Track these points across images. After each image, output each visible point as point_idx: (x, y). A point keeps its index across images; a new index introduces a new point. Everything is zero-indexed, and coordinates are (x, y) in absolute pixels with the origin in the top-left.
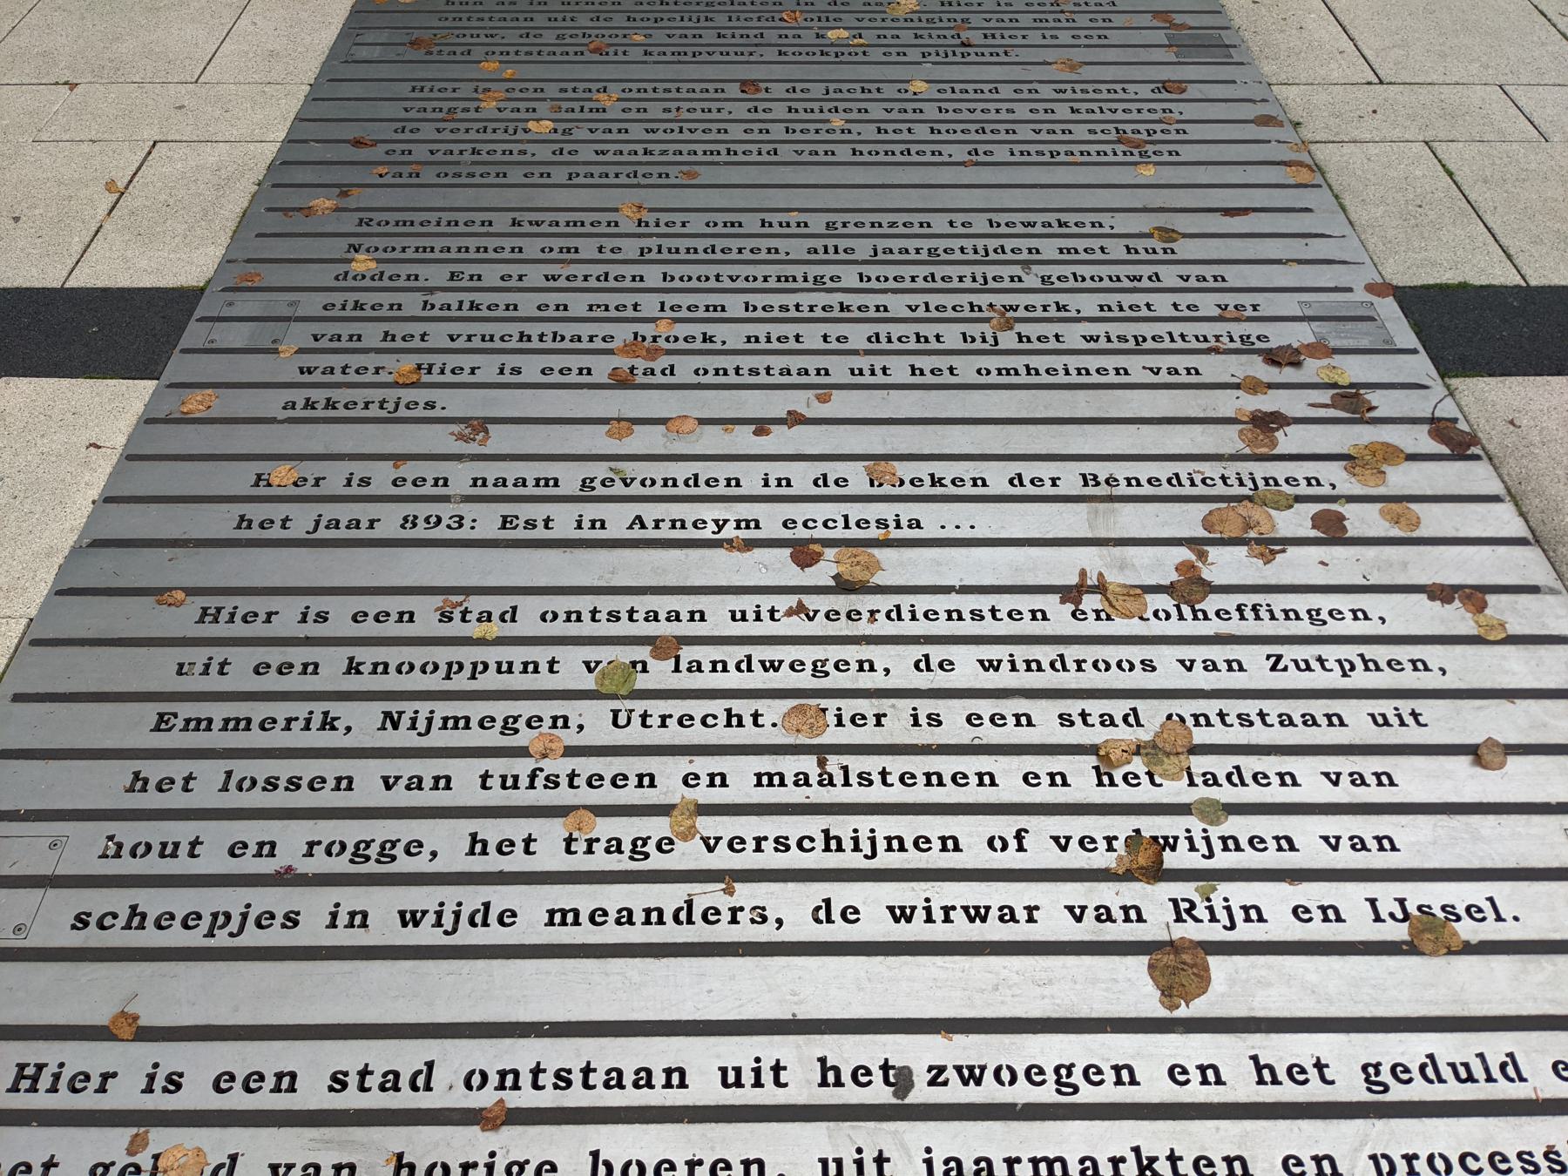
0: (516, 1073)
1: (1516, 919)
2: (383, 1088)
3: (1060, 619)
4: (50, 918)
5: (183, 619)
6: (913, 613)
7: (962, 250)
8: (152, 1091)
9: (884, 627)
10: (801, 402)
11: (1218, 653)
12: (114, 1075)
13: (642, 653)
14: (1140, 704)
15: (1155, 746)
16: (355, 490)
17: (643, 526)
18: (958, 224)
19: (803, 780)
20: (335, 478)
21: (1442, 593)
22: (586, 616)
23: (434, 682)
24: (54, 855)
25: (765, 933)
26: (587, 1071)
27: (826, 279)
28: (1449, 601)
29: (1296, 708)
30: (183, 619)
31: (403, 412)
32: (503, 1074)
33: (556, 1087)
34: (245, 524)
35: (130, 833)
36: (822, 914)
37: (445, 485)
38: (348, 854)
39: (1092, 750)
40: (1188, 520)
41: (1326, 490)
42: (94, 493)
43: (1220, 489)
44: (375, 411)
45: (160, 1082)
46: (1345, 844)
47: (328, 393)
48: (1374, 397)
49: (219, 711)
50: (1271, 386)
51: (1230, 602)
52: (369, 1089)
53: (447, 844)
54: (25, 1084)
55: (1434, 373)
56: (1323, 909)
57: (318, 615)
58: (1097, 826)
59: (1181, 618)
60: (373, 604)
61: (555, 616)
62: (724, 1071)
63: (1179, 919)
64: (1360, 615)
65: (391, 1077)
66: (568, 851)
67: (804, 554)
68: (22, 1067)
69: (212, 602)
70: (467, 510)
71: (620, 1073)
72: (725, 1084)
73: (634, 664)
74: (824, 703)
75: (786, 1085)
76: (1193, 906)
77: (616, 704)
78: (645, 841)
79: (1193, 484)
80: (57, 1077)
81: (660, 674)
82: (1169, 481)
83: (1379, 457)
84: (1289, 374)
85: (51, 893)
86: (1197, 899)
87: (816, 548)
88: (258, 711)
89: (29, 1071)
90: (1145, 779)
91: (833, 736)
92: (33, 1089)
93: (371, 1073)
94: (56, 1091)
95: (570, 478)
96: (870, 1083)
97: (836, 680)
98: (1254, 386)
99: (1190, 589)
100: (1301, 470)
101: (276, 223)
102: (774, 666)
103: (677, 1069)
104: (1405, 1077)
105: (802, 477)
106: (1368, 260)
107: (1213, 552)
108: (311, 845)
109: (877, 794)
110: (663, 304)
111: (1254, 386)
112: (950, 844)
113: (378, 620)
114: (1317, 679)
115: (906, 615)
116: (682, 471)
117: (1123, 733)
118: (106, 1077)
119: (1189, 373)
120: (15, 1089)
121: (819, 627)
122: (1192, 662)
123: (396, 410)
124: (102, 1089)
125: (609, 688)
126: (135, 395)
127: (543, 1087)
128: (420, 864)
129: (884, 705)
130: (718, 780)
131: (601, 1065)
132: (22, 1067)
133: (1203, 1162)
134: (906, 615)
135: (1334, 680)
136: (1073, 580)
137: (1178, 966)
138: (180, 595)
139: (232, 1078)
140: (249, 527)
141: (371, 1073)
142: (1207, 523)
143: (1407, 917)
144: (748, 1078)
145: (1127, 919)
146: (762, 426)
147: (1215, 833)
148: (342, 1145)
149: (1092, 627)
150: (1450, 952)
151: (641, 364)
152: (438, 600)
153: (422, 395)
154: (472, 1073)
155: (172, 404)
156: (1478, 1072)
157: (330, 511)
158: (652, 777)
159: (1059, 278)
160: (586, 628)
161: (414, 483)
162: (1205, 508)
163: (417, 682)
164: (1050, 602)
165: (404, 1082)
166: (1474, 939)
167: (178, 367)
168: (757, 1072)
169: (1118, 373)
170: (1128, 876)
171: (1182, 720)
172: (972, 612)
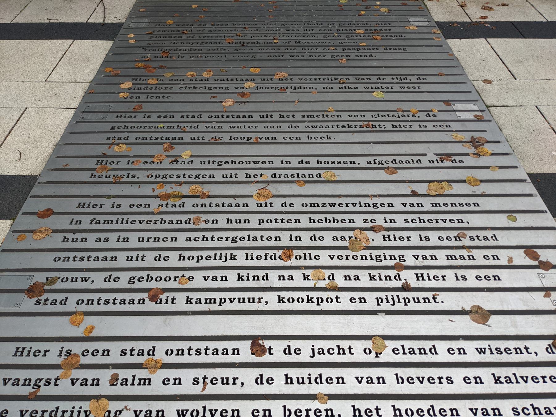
0: (183, 350)
2: (138, 355)
12: (49, 351)
18: (340, 127)
22: (208, 205)
30: (111, 117)
33: (196, 354)
34: (66, 240)
36: (287, 351)
54: (19, 354)
57: (118, 205)
61: (197, 206)
68: (18, 348)
69: (21, 344)
71: (217, 350)
75: (353, 354)
80: (29, 351)
89: (20, 350)
92: (22, 355)
101: (61, 163)
110: (231, 137)
118: (46, 351)
122: (418, 256)
132: (18, 348)
140: (95, 177)
144: (306, 381)
154: (168, 350)
156: (513, 380)
158: (226, 277)
159: (385, 162)
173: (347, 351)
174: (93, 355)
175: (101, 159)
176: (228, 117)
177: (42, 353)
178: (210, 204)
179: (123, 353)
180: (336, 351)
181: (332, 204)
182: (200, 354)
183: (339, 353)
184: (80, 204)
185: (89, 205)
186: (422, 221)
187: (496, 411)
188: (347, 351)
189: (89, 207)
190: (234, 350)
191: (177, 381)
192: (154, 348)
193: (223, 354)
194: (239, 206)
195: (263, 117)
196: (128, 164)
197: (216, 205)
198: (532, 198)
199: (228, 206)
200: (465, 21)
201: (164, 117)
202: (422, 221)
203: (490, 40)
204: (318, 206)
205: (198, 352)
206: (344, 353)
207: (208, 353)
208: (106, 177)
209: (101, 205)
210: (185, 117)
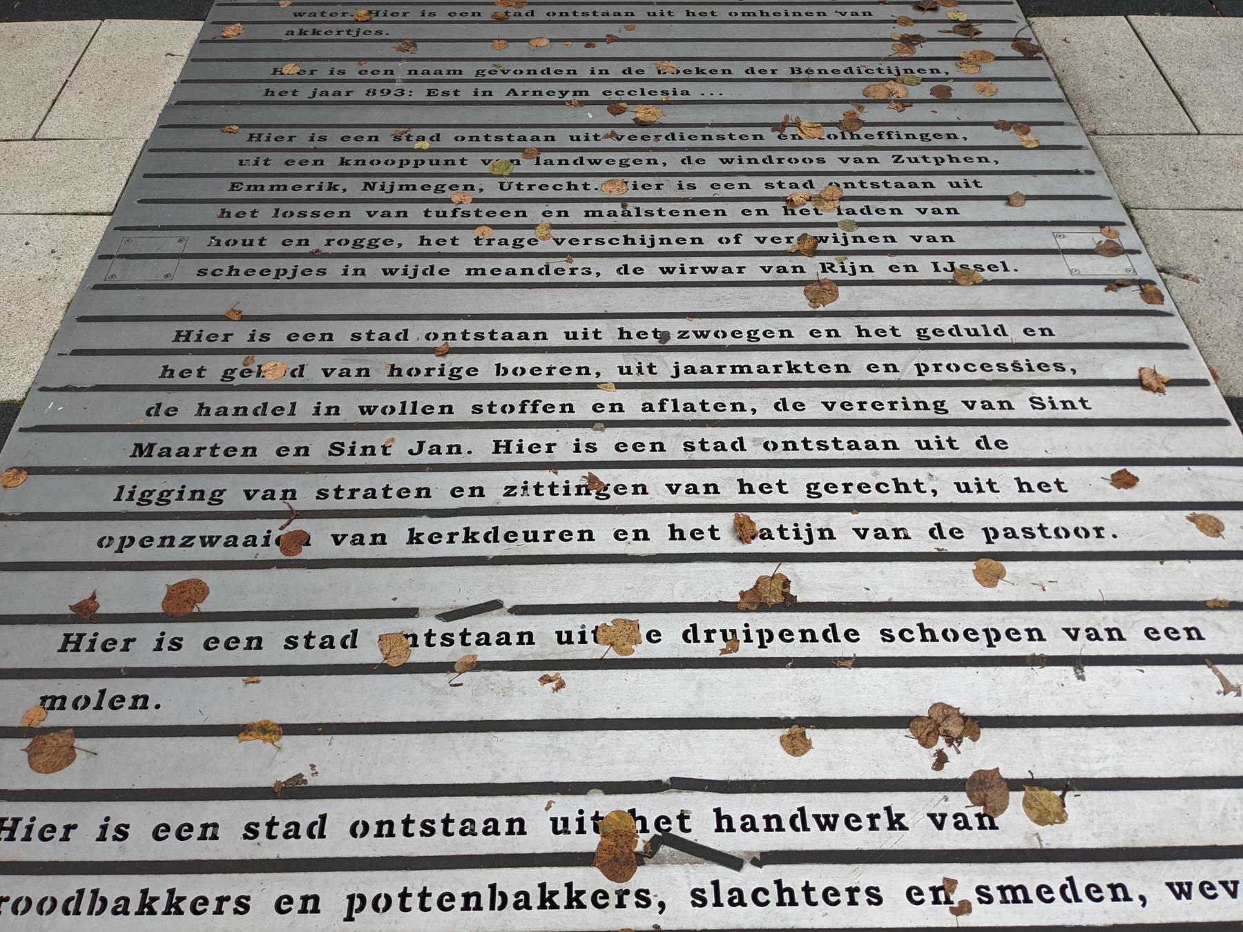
0: (391, 824)
2: (286, 836)
3: (771, 138)
5: (241, 139)
8: (104, 839)
9: (663, 143)
10: (614, 30)
11: (863, 155)
13: (518, 156)
14: (814, 179)
15: (820, 197)
16: (335, 76)
17: (515, 94)
19: (613, 214)
20: (323, 70)
21: (1003, 126)
23: (395, 169)
24: (182, 244)
25: (591, 278)
26: (447, 821)
28: (1008, 129)
29: (906, 180)
31: (361, 36)
32: (380, 824)
33: (422, 834)
35: (224, 236)
37: (331, 339)
38: (351, 244)
39: (784, 199)
40: (855, 91)
41: (943, 75)
42: (175, 79)
43: (877, 75)
44: (344, 36)
45: (110, 833)
47: (314, 26)
48: (980, 27)
49: (267, 182)
50: (915, 21)
51: (874, 131)
52: (275, 837)
53: (409, 241)
55: (1021, 15)
58: (782, 233)
59: (844, 138)
60: (354, 133)
63: (824, 271)
65: (292, 827)
66: (477, 244)
67: (615, 108)
68: (67, 636)
70: (407, 87)
71: (487, 636)
72: (555, 831)
73: (512, 161)
74: (626, 179)
76: (833, 265)
77: (502, 180)
79: (860, 72)
80: (30, 828)
81: (528, 166)
83: (978, 58)
84: (929, 15)
85: (182, 260)
86: (835, 263)
87: (624, 105)
88: (291, 182)
89: (71, 647)
90: (812, 212)
91: (632, 194)
92: (77, 649)
93: (277, 824)
94: (29, 840)
95: (469, 70)
97: (633, 168)
98: (906, 22)
99: (850, 126)
100: (927, 65)
102: (597, 162)
104: (1047, 897)
105: (616, 70)
106: (1128, 221)
107: (867, 107)
109: (656, 219)
111: (906, 22)
114: (922, 166)
116: (540, 66)
117: (803, 192)
121: (625, 143)
123: (294, 276)
125: (496, 172)
126: (193, 29)
127: (412, 835)
128: (393, 249)
129: (662, 180)
131: (458, 818)
132: (67, 636)
133: (914, 891)
135: (932, 166)
136: (781, 120)
137: (820, 291)
138: (235, 128)
139: (168, 828)
141: (277, 824)
142: (865, 93)
143: (953, 269)
144: (573, 826)
146: (590, 43)
147: (849, 235)
148: (360, 361)
149: (790, 142)
150: (975, 284)
151: (512, 10)
152: (392, 131)
153: (374, 27)
154: (356, 823)
155: (214, 32)
157: (321, 87)
160: (483, 144)
161: (305, 338)
162: (865, 85)
163: (382, 168)
164: (766, 132)
166: (990, 279)
167: (215, 13)
168: (583, 634)
170: (797, 253)
171: (838, 185)
173: (800, 896)
174: (180, 838)
176: (499, 138)
177: (121, 644)
178: (465, 333)
179: (291, 643)
180: (773, 897)
181: (668, 269)
182: (452, 643)
183: (781, 903)
184: (179, 333)
185: (199, 336)
187: (1119, 890)
188: (800, 896)
189: (199, 340)
190: (521, 635)
191: (386, 828)
192: (355, 632)
193: (499, 643)
195: (578, 139)
197: (476, 334)
198: (1185, 351)
201: (356, 139)
203: (1136, 19)
205: (428, 828)
206: (793, 903)
207: (450, 831)
208: (244, 244)
209: (226, 335)
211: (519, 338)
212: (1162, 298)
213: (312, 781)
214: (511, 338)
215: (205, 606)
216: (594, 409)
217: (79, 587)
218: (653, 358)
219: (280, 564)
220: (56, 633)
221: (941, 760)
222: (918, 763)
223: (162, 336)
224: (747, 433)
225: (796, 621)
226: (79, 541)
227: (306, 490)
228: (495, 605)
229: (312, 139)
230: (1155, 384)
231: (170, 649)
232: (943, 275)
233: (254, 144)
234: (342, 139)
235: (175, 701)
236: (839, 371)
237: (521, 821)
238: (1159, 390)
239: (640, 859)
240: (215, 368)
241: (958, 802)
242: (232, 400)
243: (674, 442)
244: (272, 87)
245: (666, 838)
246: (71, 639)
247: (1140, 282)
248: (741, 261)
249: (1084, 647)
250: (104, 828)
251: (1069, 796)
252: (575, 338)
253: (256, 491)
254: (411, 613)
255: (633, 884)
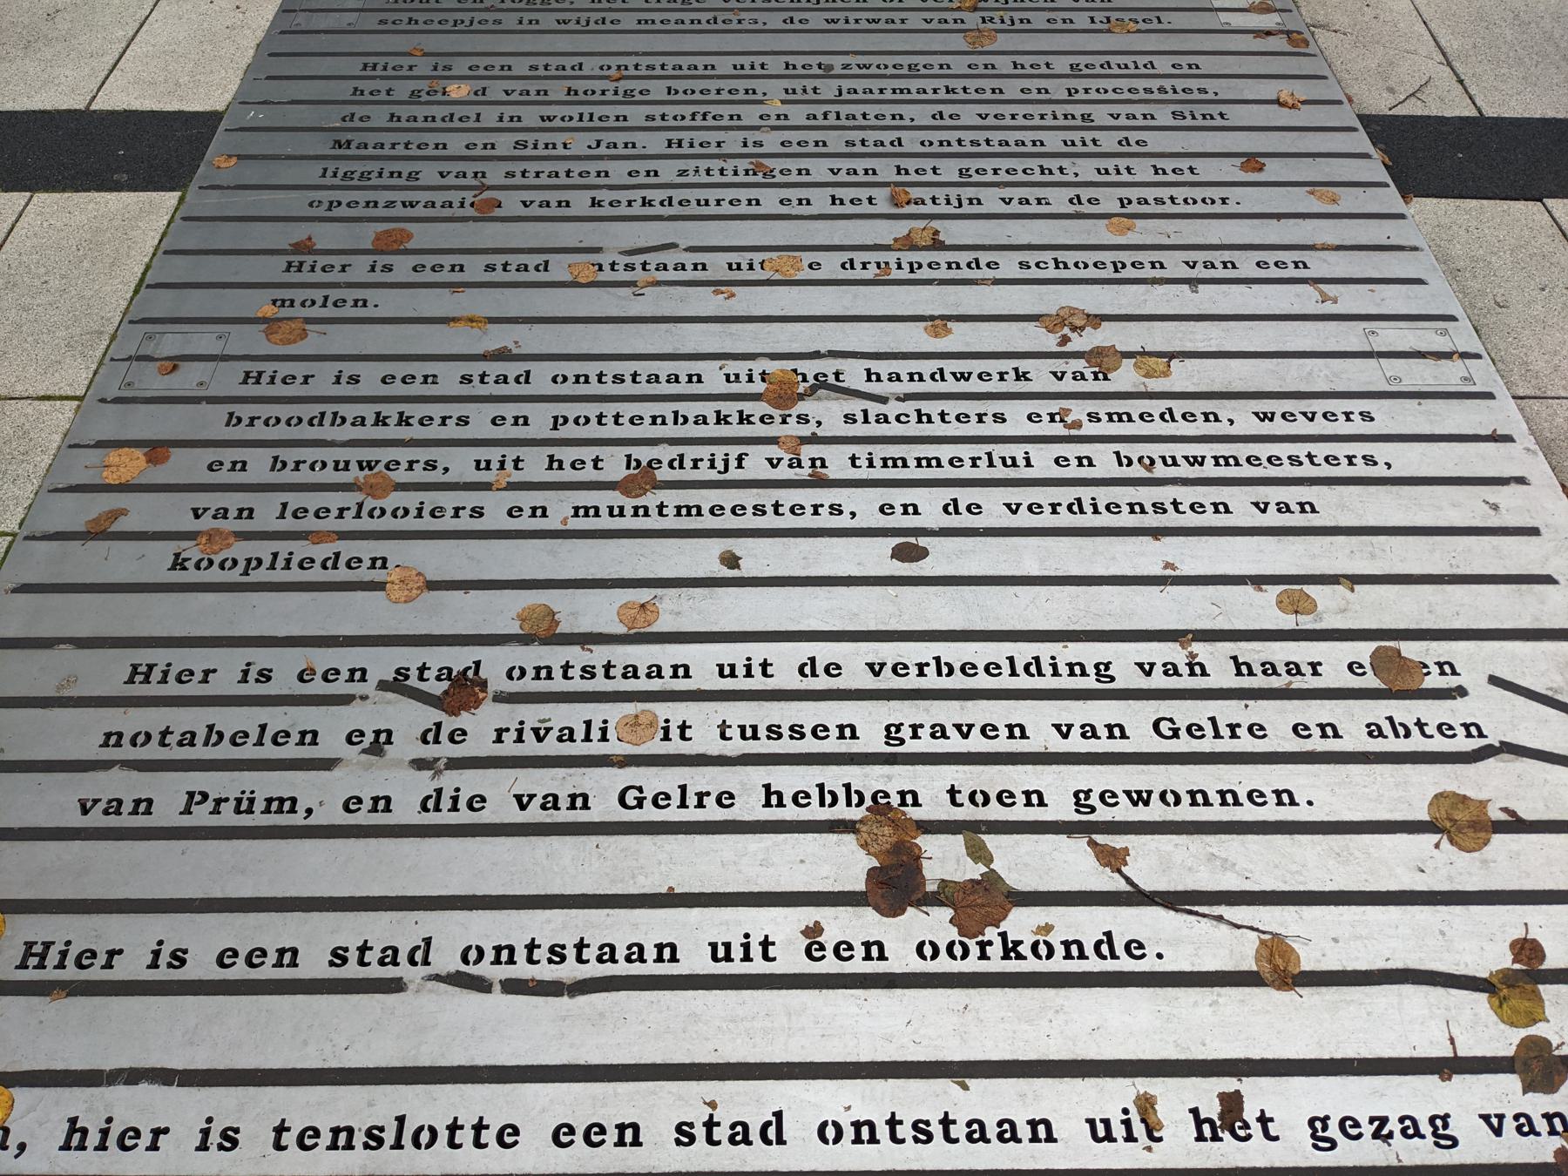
0: (511, 949)
1: (1310, 803)
4: (54, 801)
6: (1095, 506)
7: (988, 142)
8: (157, 967)
12: (120, 952)
18: (871, 116)
22: (557, 673)
24: (222, 342)
27: (972, 172)
31: (476, 26)
32: (498, 950)
33: (550, 961)
46: (1076, 732)
54: (33, 961)
56: (1278, 793)
62: (714, 946)
64: (1307, 508)
65: (389, 952)
68: (135, 667)
71: (613, 948)
72: (715, 958)
75: (774, 959)
78: (898, 727)
80: (64, 954)
82: (932, 377)
89: (38, 949)
92: (258, 382)
96: (823, 957)
103: (668, 945)
108: (500, 732)
112: (1017, 731)
113: (318, 517)
115: (1088, 509)
119: (1225, 267)
120: (23, 966)
124: (108, 965)
126: (172, 198)
127: (538, 962)
130: (681, 671)
131: (594, 941)
132: (135, 667)
134: (1088, 509)
139: (235, 954)
145: (1224, 803)
154: (470, 947)
165: (403, 957)
169: (1153, 267)
170: (959, 9)
172: (1154, 505)
175: (296, 259)
176: (618, 379)
178: (600, 376)
184: (247, 374)
186: (1244, 669)
189: (164, 681)
191: (505, 955)
194: (677, 381)
196: (338, 382)
199: (648, 382)
200: (1466, 114)
202: (1244, 669)
204: (905, 465)
209: (207, 673)
210: (499, 268)
211: (649, 676)
212: (1307, 44)
213: (515, 351)
214: (635, 676)
215: (410, 245)
216: (494, 422)
217: (299, 232)
218: (817, 83)
219: (475, 219)
220: (282, 261)
221: (1065, 340)
222: (1050, 342)
223: (353, 66)
224: (903, 134)
225: (942, 257)
226: (296, 203)
227: (495, 174)
228: (673, 246)
229: (373, 269)
230: (1290, 102)
231: (257, 681)
232: (1098, 26)
233: (251, 390)
234: (415, 269)
235: (388, 303)
236: (1080, 464)
237: (673, 947)
238: (1293, 107)
239: (801, 397)
240: (403, 90)
241: (1079, 365)
242: (420, 111)
243: (836, 141)
244: (361, 84)
245: (826, 386)
246: (141, 678)
247: (1288, 33)
248: (903, 15)
249: (1201, 272)
250: (156, 954)
251: (1174, 363)
252: (733, 675)
253: (96, 801)
254: (598, 250)
255: (795, 411)
